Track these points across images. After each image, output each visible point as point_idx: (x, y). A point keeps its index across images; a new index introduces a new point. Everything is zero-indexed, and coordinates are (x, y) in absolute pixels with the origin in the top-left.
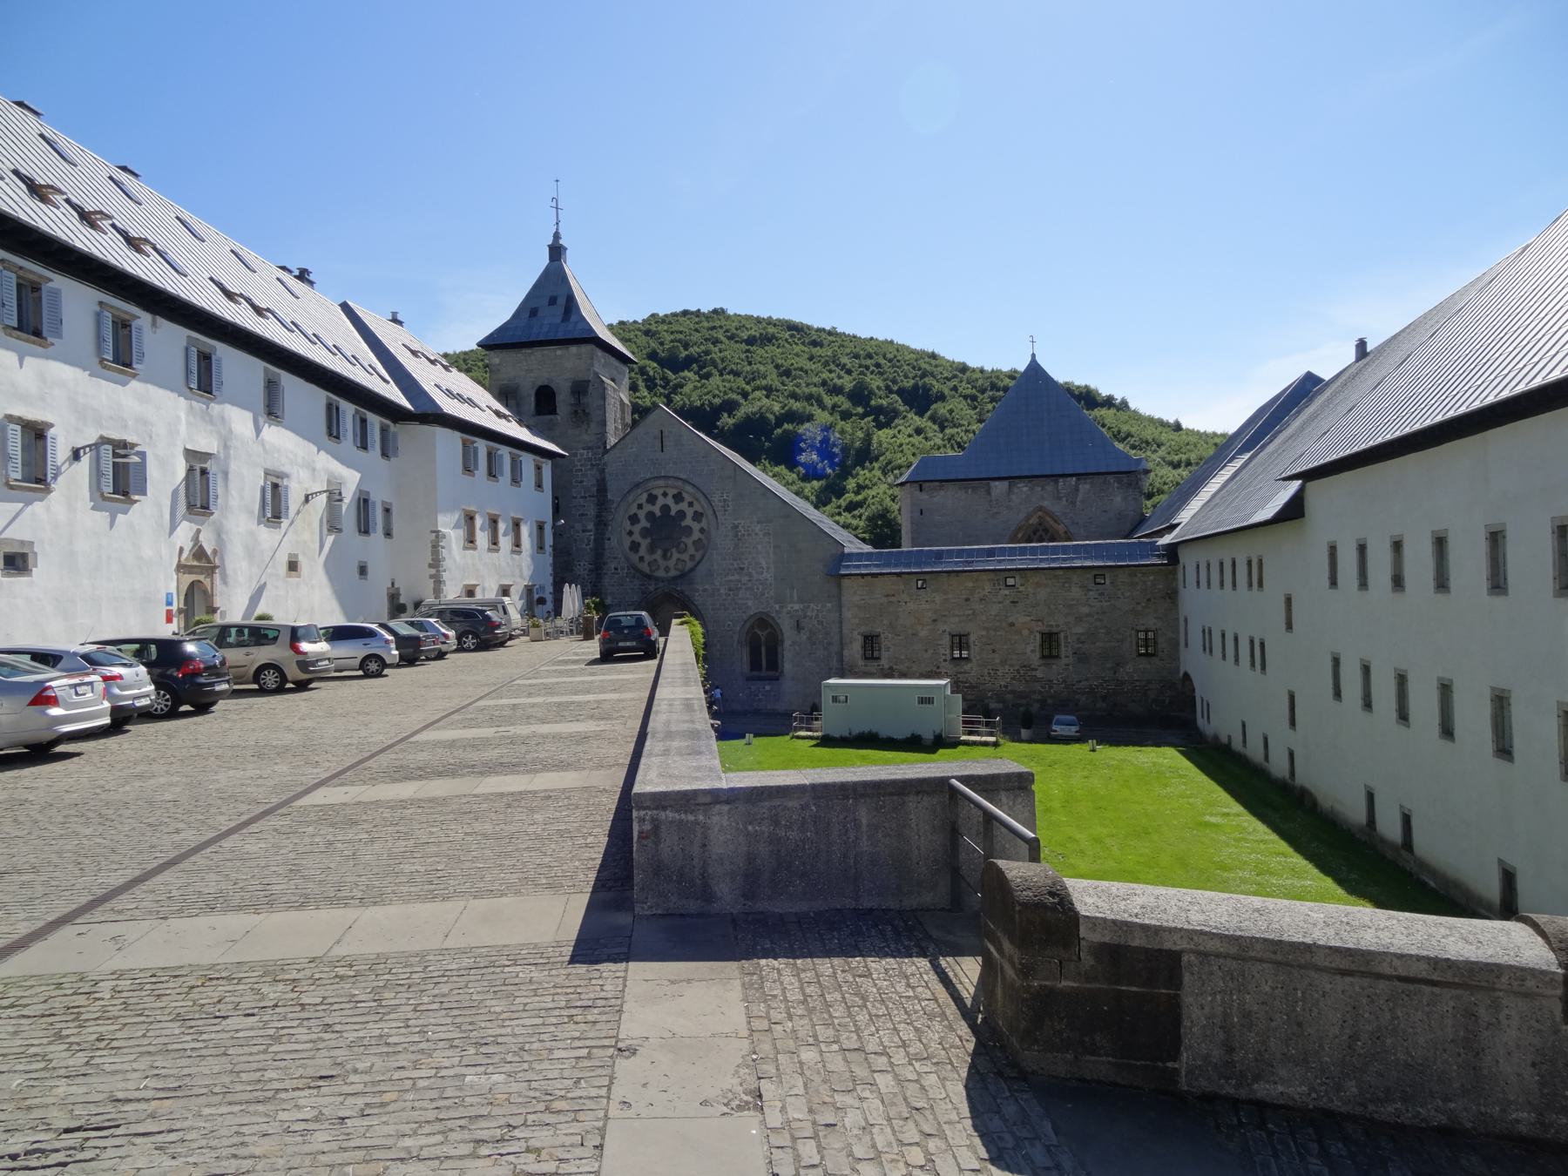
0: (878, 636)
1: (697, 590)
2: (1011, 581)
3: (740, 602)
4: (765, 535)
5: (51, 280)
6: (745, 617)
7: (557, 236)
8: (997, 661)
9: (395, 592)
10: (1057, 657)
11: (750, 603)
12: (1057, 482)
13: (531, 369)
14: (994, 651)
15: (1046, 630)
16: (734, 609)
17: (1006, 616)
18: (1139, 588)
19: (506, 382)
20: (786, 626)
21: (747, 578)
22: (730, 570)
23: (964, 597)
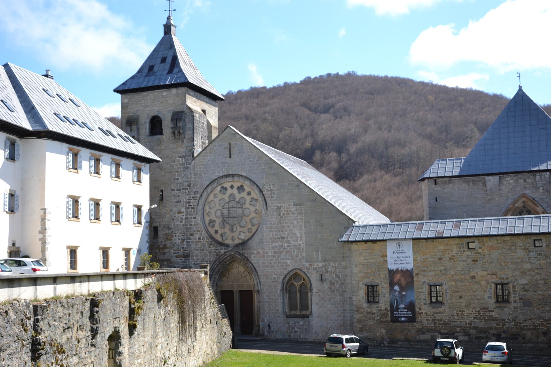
1: (253, 253)
4: (298, 214)
6: (285, 272)
7: (169, 18)
8: (463, 304)
9: (17, 250)
10: (507, 301)
11: (289, 262)
12: (535, 176)
14: (461, 297)
15: (499, 281)
16: (278, 266)
19: (131, 114)
21: (286, 245)
22: (275, 238)
23: (439, 256)
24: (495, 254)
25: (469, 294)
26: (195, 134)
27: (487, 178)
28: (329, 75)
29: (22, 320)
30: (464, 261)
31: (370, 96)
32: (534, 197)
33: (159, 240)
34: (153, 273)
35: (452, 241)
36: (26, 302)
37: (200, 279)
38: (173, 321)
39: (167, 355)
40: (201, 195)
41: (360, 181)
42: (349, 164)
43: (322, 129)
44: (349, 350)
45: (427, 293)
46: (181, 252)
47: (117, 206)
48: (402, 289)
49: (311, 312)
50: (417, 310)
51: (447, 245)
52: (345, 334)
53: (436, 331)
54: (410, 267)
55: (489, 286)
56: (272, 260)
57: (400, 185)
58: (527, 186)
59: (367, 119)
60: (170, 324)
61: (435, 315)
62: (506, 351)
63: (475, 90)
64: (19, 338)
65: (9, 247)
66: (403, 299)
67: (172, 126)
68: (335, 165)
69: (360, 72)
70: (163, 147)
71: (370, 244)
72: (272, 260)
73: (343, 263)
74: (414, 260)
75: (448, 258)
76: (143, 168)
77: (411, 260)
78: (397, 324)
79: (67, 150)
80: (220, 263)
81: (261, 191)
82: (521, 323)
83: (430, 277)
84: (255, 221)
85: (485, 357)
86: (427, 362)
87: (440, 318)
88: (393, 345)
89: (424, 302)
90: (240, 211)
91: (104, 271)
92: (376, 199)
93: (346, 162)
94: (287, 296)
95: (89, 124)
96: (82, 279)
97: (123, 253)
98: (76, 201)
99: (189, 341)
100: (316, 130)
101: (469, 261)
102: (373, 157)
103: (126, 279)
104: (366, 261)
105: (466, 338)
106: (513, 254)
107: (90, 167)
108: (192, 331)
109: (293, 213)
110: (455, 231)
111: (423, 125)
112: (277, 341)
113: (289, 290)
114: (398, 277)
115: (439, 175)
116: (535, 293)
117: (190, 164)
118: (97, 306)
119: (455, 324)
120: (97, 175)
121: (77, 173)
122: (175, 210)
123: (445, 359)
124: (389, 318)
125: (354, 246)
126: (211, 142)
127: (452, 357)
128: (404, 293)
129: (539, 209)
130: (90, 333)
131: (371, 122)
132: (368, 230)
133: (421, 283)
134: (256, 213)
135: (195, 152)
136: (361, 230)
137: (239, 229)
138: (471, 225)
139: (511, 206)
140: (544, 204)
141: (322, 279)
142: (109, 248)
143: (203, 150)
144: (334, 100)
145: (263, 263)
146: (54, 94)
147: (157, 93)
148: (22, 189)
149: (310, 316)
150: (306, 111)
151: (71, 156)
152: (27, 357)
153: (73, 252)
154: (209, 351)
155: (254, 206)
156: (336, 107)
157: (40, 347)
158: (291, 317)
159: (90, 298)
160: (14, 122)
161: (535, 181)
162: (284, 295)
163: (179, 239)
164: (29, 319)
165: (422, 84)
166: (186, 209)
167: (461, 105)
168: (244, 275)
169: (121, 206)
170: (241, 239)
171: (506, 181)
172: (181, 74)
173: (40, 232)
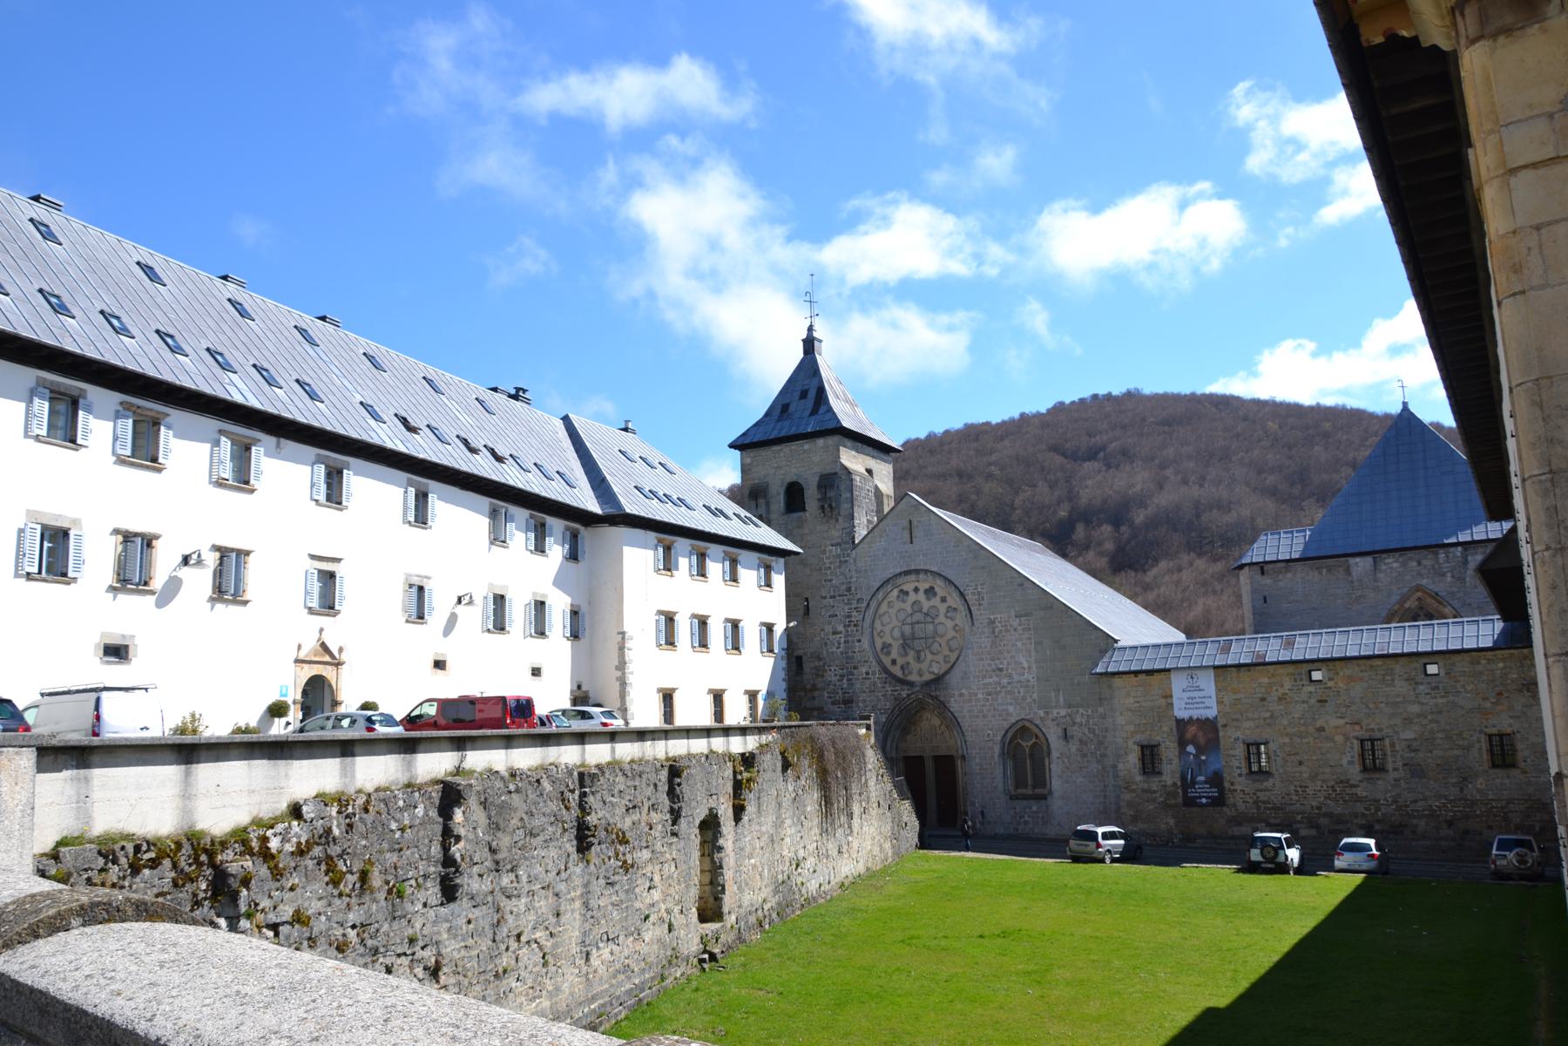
0: (1158, 746)
2: (1316, 675)
3: (1000, 708)
4: (1024, 630)
5: (168, 415)
6: (1006, 726)
7: (810, 329)
8: (1305, 775)
10: (1383, 769)
11: (1011, 709)
12: (1436, 554)
13: (787, 465)
14: (1301, 763)
15: (1366, 735)
16: (994, 716)
17: (1314, 719)
18: (1485, 678)
19: (756, 481)
20: (1053, 735)
22: (987, 671)
23: (1261, 695)
24: (1357, 690)
25: (1314, 758)
26: (856, 509)
27: (1352, 561)
28: (1095, 397)
29: (562, 793)
30: (1303, 702)
31: (1166, 428)
32: (1436, 590)
33: (805, 677)
34: (773, 728)
35: (1281, 670)
36: (567, 767)
37: (857, 736)
38: (810, 801)
39: (801, 853)
40: (869, 604)
41: (1154, 571)
42: (1133, 543)
43: (1087, 487)
44: (1109, 851)
45: (1242, 757)
46: (839, 696)
47: (735, 625)
48: (1200, 750)
49: (1051, 790)
50: (1227, 785)
51: (1273, 676)
52: (1101, 825)
53: (1260, 821)
54: (1211, 713)
55: (1348, 744)
56: (984, 706)
57: (1224, 576)
58: (1424, 571)
59: (1162, 467)
60: (804, 806)
61: (1258, 794)
62: (1374, 852)
63: (1352, 409)
64: (557, 819)
65: (572, 691)
66: (1203, 768)
67: (819, 496)
68: (1109, 546)
69: (1148, 389)
70: (806, 531)
71: (1142, 677)
72: (984, 706)
73: (1101, 710)
74: (1218, 702)
75: (1276, 698)
76: (773, 564)
77: (1213, 702)
78: (1194, 809)
79: (656, 542)
80: (901, 712)
81: (962, 595)
82: (1408, 806)
83: (1246, 730)
84: (954, 644)
85: (1338, 863)
86: (1238, 871)
87: (1266, 799)
88: (1190, 845)
89: (1239, 771)
90: (930, 627)
91: (717, 725)
92: (1182, 601)
93: (1128, 542)
94: (1010, 764)
95: (688, 501)
96: (656, 735)
97: (710, 698)
98: (670, 619)
99: (840, 832)
100: (1076, 489)
101: (1313, 701)
102: (1175, 530)
103: (728, 736)
104: (1137, 705)
105: (1313, 832)
106: (1387, 689)
107: (691, 566)
108: (843, 819)
109: (1015, 630)
110: (1222, 656)
111: (1260, 472)
112: (995, 837)
113: (1014, 755)
114: (1192, 730)
115: (1267, 559)
116: (1429, 755)
117: (848, 555)
118: (680, 776)
119: (1293, 808)
120: (702, 578)
121: (672, 576)
122: (828, 629)
123: (1269, 866)
124: (1180, 800)
125: (1117, 681)
126: (882, 518)
127: (1280, 863)
128: (1203, 758)
129: (1447, 610)
130: (668, 815)
131: (1169, 472)
132: (1150, 654)
133: (1232, 740)
134: (957, 631)
135: (856, 535)
136: (1128, 655)
137: (930, 657)
138: (1312, 641)
139: (1396, 607)
140: (1455, 602)
141: (1066, 736)
142: (674, 690)
143: (868, 533)
144: (1105, 438)
145: (969, 711)
146: (636, 457)
147: (794, 446)
148: (589, 603)
149: (1049, 798)
150: (1059, 459)
151: (661, 550)
152: (571, 847)
153: (668, 697)
154: (876, 851)
155: (952, 619)
156: (1108, 450)
157: (590, 833)
158: (1017, 799)
159: (668, 764)
160: (575, 504)
161: (1438, 562)
162: (1004, 764)
163: (836, 675)
164: (572, 791)
165: (1257, 403)
166: (845, 626)
167: (1326, 435)
168: (940, 732)
169: (741, 625)
170: (933, 673)
171: (1385, 564)
172: (830, 414)
173: (617, 668)
